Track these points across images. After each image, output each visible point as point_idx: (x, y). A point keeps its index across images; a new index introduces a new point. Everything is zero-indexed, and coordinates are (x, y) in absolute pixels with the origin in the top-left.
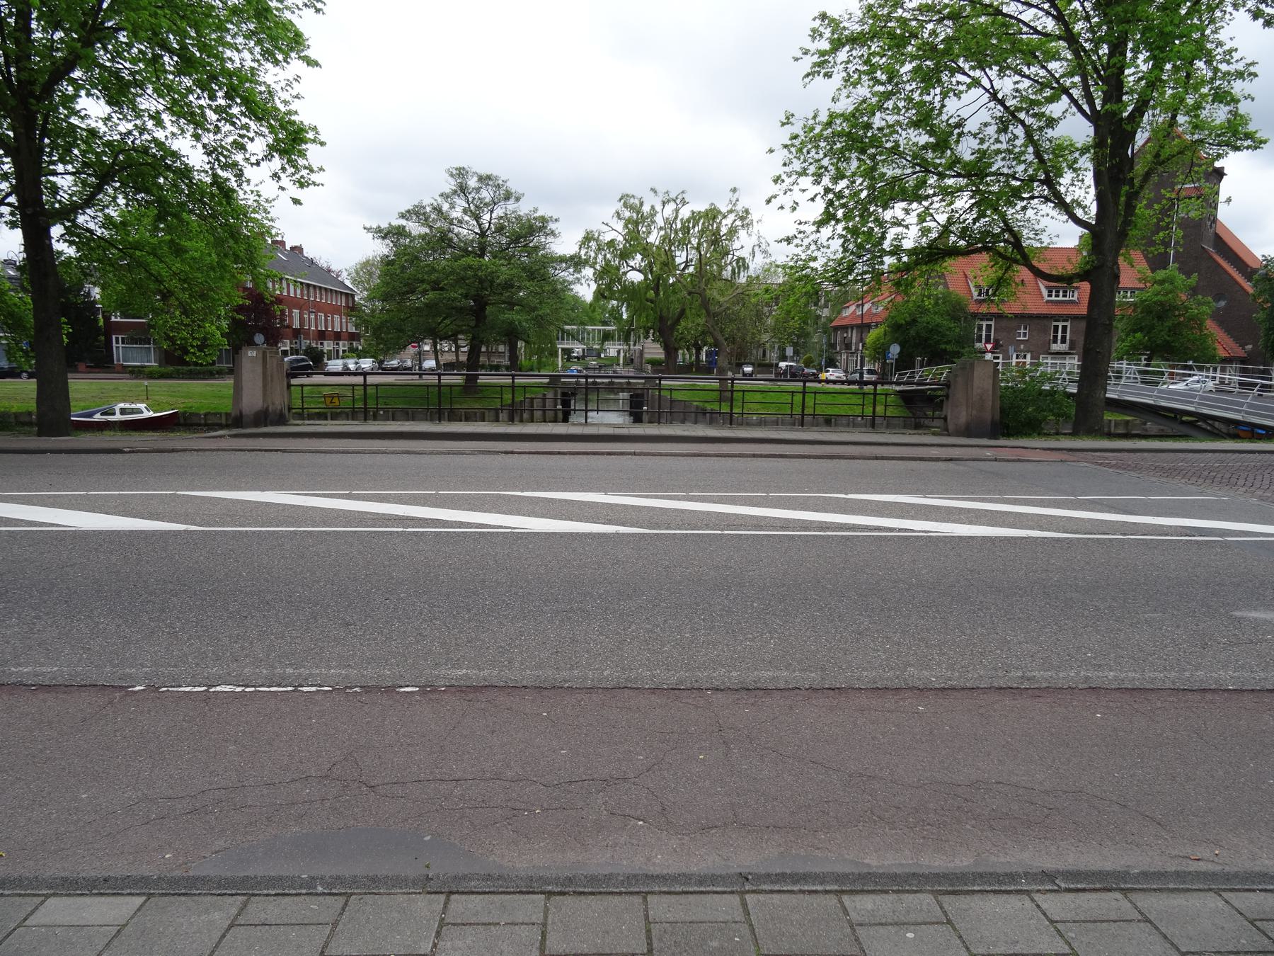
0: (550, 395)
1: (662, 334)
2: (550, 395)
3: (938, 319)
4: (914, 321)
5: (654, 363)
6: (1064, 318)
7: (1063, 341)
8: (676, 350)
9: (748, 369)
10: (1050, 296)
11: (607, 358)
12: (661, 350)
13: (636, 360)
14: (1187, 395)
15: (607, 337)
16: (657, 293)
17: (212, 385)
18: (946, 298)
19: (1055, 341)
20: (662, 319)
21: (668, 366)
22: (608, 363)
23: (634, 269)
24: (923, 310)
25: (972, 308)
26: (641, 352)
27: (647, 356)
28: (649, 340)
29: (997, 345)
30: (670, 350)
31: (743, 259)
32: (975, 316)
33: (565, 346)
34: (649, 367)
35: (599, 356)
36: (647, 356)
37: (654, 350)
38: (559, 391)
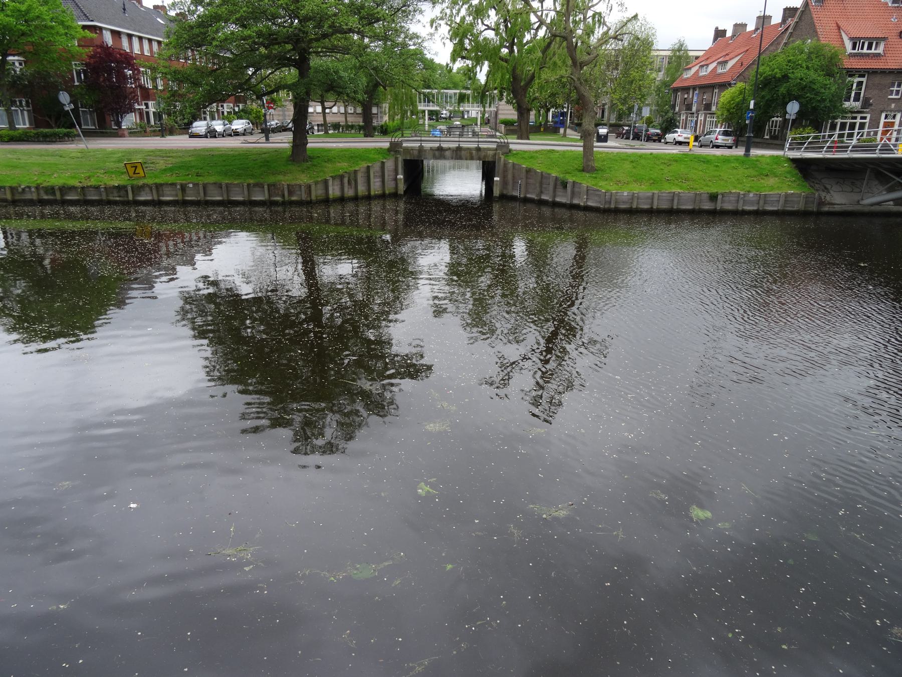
0: (389, 165)
1: (515, 97)
2: (389, 165)
3: (812, 75)
4: (785, 77)
5: (507, 123)
6: (861, 73)
7: (857, 99)
8: (529, 110)
9: (603, 131)
10: (854, 48)
11: (470, 119)
12: (516, 113)
13: (492, 121)
14: (532, 155)
15: (462, 98)
16: (511, 51)
17: (14, 152)
18: (816, 52)
19: (848, 99)
20: (515, 78)
21: (521, 129)
22: (469, 123)
23: (489, 28)
24: (796, 65)
25: (849, 64)
26: (496, 113)
27: (501, 117)
28: (503, 102)
29: (866, 104)
30: (523, 111)
31: (600, 14)
32: (851, 73)
33: (431, 108)
34: (503, 126)
35: (463, 117)
36: (501, 117)
37: (508, 112)
38: (400, 159)
